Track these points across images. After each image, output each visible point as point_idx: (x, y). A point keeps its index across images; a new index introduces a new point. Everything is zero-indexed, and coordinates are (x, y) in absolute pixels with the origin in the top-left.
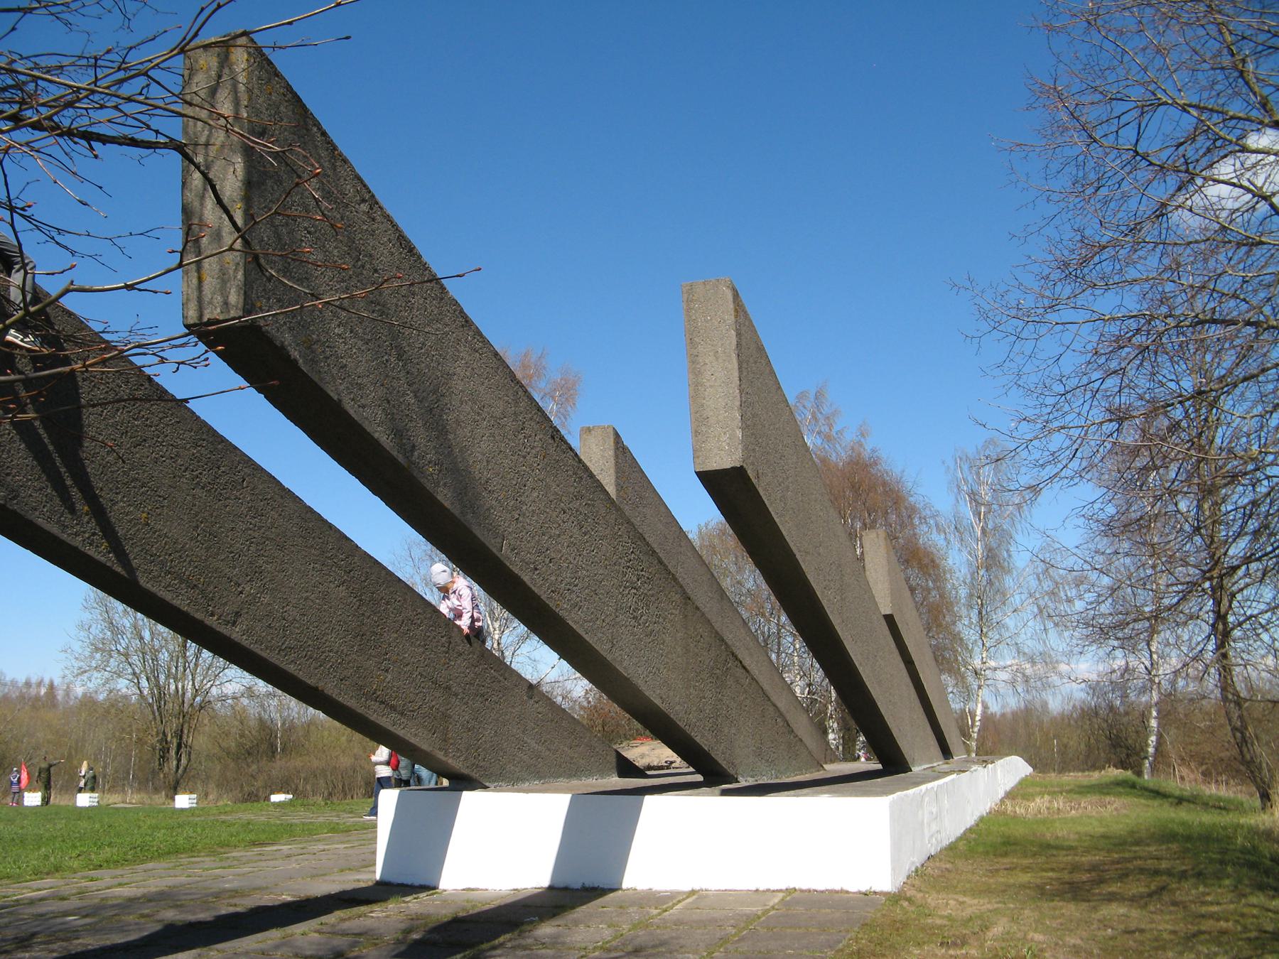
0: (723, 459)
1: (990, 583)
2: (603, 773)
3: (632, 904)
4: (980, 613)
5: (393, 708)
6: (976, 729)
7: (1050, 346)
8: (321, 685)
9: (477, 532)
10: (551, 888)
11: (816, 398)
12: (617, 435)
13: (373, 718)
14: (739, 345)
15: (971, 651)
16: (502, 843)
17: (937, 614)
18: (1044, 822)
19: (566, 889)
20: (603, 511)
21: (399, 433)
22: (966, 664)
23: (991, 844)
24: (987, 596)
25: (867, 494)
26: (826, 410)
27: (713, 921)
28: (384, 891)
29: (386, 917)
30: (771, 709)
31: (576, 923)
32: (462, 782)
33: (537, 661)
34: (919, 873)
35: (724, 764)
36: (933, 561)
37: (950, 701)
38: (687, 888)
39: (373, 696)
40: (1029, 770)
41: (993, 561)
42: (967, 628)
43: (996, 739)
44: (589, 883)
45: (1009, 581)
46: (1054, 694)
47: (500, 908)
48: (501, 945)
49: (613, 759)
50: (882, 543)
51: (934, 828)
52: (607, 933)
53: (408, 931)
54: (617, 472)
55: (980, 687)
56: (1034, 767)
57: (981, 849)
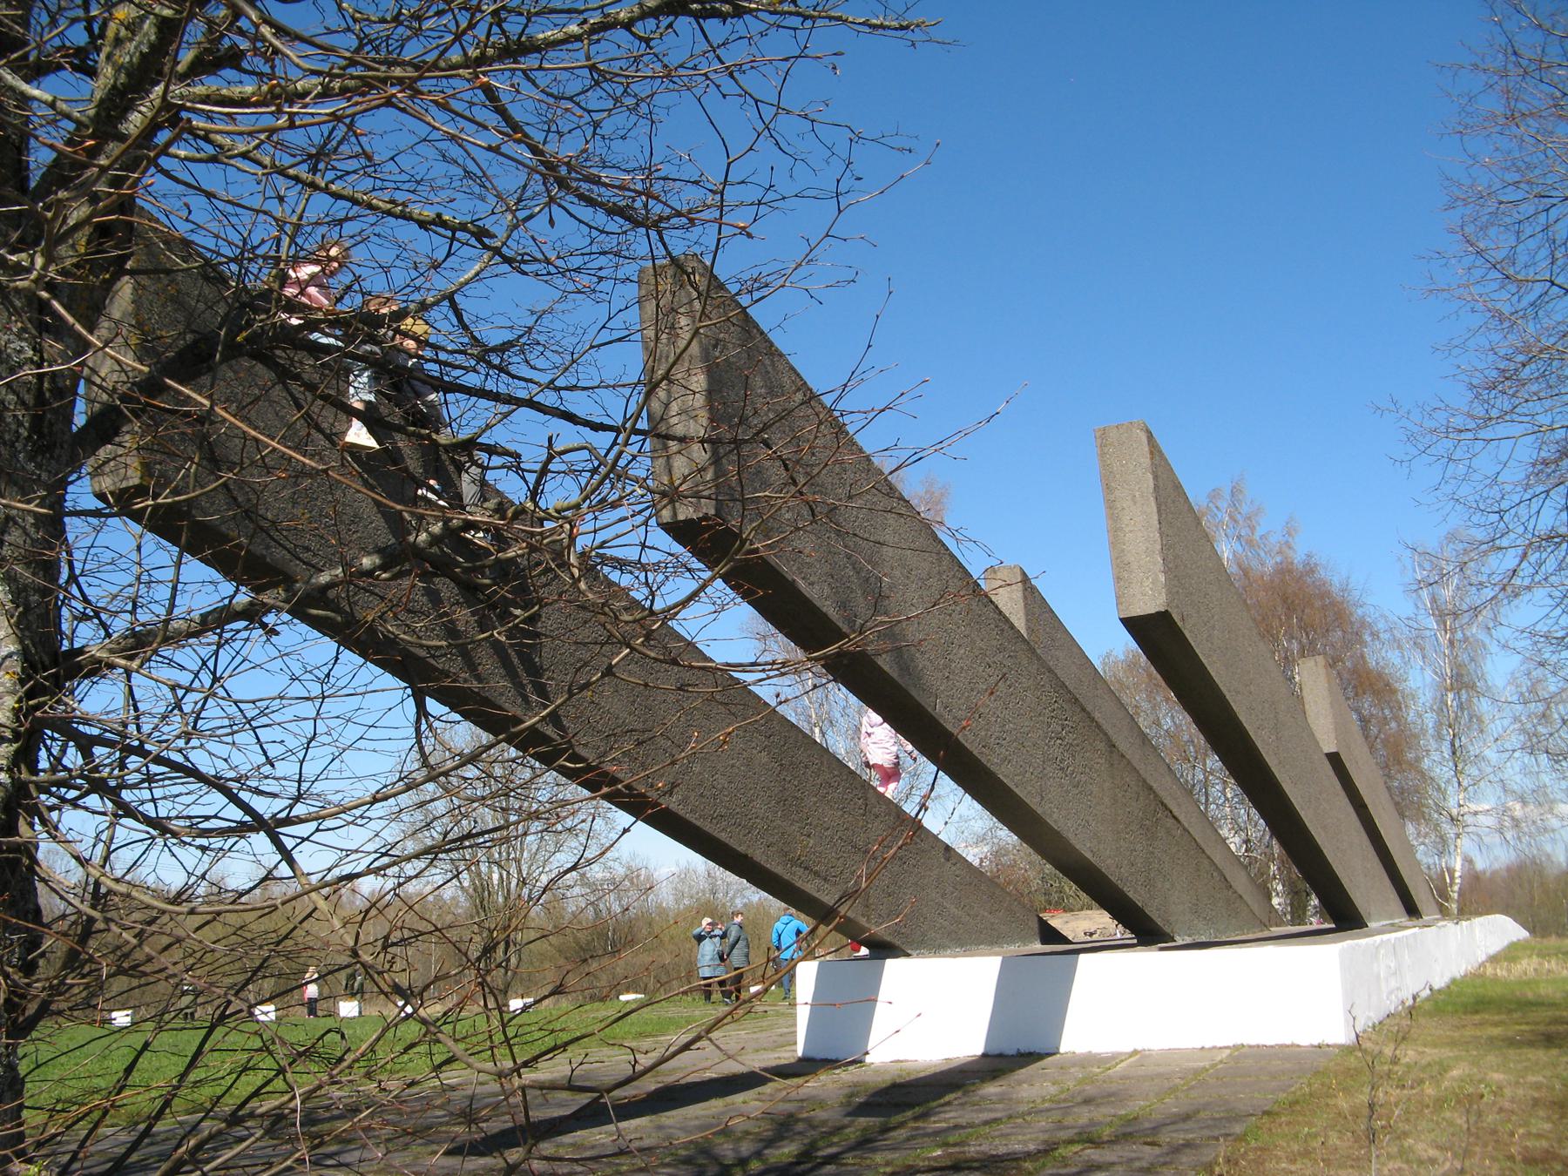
0: (1148, 602)
1: (1461, 707)
2: (1025, 940)
3: (1074, 1065)
4: (1453, 745)
5: (817, 874)
6: (1456, 888)
7: (1485, 463)
8: (750, 852)
9: (914, 693)
10: (984, 1055)
11: (1233, 494)
12: (1025, 579)
13: (799, 884)
14: (1156, 487)
15: (1444, 793)
16: (930, 1011)
17: (1396, 752)
18: (1528, 983)
19: (1000, 1056)
20: (1025, 662)
21: (843, 605)
22: (1439, 809)
23: (1467, 1004)
24: (1458, 723)
25: (1304, 611)
26: (1245, 509)
27: (1159, 1075)
28: (808, 1066)
29: (822, 1084)
30: (1206, 861)
31: (1020, 1083)
32: (883, 949)
33: (958, 820)
34: (1378, 1027)
35: (1159, 922)
36: (1388, 684)
37: (1418, 852)
38: (1129, 1049)
39: (795, 862)
40: (1523, 934)
41: (1461, 681)
42: (1437, 763)
43: (1479, 896)
44: (1024, 1048)
45: (1484, 706)
46: (1553, 840)
47: (935, 1075)
48: (948, 1103)
49: (1035, 925)
50: (1322, 671)
51: (1393, 984)
52: (1053, 1090)
53: (851, 1095)
54: (1027, 615)
55: (1458, 836)
56: (1532, 931)
57: (1450, 1008)
